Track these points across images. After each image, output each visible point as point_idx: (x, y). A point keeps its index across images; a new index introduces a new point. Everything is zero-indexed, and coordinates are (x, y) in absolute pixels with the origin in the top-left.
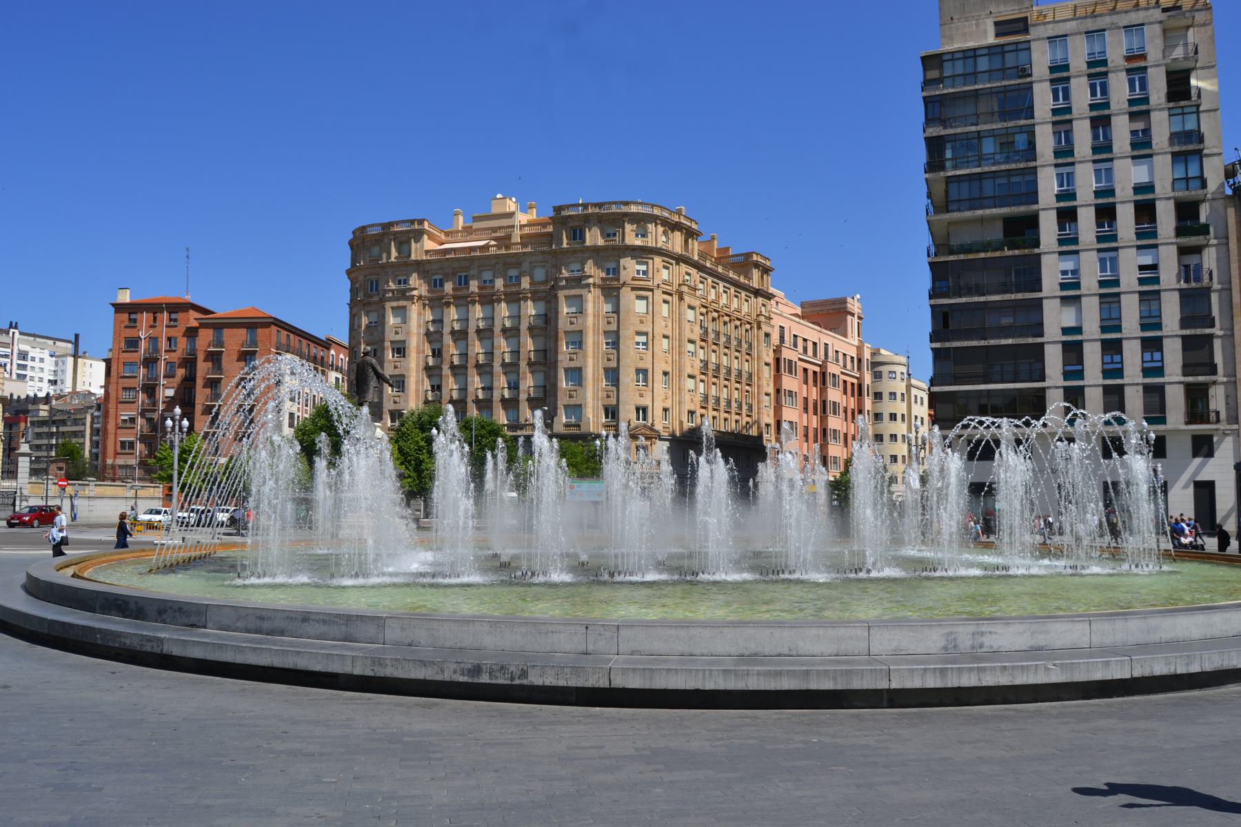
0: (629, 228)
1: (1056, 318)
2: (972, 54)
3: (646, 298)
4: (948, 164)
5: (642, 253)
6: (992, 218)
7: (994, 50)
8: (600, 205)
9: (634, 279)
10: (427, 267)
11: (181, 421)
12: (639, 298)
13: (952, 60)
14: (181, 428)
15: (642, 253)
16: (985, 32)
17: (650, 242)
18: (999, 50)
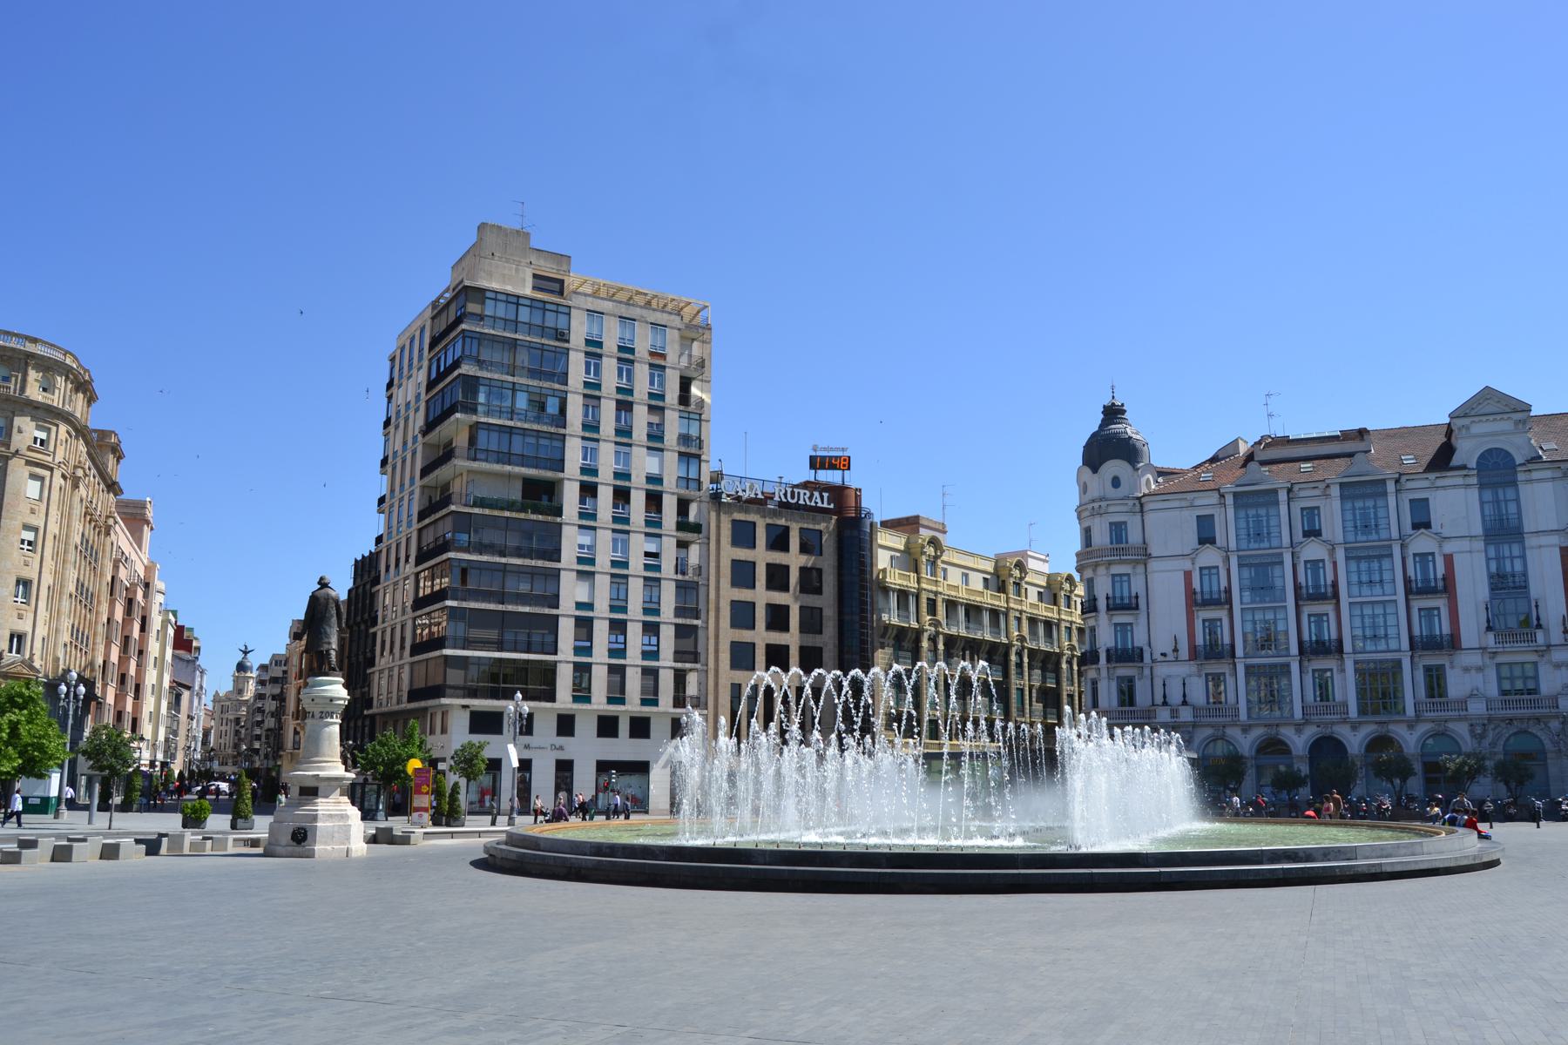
0: (33, 375)
1: (572, 591)
3: (42, 479)
5: (46, 414)
12: (33, 476)
15: (46, 414)
17: (55, 400)
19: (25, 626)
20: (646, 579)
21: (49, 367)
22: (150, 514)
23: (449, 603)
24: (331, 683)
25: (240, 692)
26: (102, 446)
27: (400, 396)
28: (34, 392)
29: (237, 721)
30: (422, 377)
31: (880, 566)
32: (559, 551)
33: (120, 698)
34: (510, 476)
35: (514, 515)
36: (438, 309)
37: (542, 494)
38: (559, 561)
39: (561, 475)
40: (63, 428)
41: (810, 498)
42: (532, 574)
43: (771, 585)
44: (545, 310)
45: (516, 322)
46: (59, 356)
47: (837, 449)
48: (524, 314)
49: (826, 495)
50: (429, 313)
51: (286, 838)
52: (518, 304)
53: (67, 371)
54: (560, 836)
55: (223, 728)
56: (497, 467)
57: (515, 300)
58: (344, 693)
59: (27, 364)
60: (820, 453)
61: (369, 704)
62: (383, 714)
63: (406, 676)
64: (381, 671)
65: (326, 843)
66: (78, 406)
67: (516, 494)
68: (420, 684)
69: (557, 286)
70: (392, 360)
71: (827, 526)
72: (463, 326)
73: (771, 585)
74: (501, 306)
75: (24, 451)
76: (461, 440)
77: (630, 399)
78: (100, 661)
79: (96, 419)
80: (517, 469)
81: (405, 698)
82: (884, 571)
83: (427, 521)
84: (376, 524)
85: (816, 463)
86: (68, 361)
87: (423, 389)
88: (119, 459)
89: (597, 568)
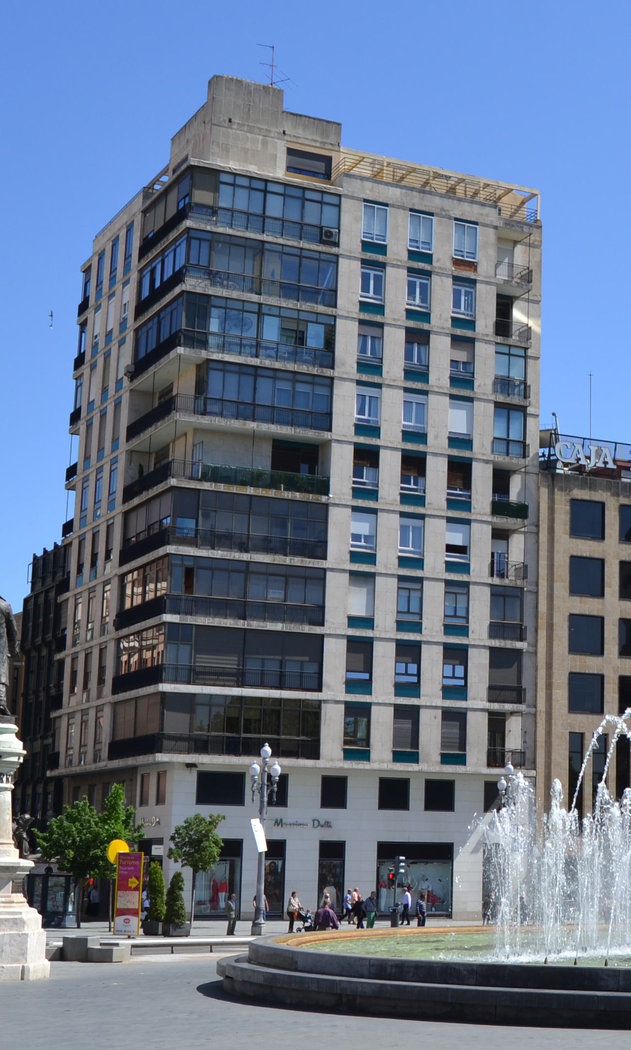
1: (343, 601)
2: (261, 186)
16: (274, 157)
18: (298, 193)
27: (98, 323)
30: (128, 295)
32: (324, 543)
35: (260, 492)
36: (153, 200)
37: (300, 462)
39: (327, 435)
52: (265, 192)
57: (262, 186)
61: (54, 761)
62: (74, 777)
63: (106, 722)
64: (71, 715)
67: (263, 462)
68: (126, 733)
69: (322, 166)
70: (87, 271)
72: (188, 223)
74: (242, 194)
76: (185, 386)
80: (264, 427)
81: (105, 753)
83: (136, 501)
87: (130, 313)
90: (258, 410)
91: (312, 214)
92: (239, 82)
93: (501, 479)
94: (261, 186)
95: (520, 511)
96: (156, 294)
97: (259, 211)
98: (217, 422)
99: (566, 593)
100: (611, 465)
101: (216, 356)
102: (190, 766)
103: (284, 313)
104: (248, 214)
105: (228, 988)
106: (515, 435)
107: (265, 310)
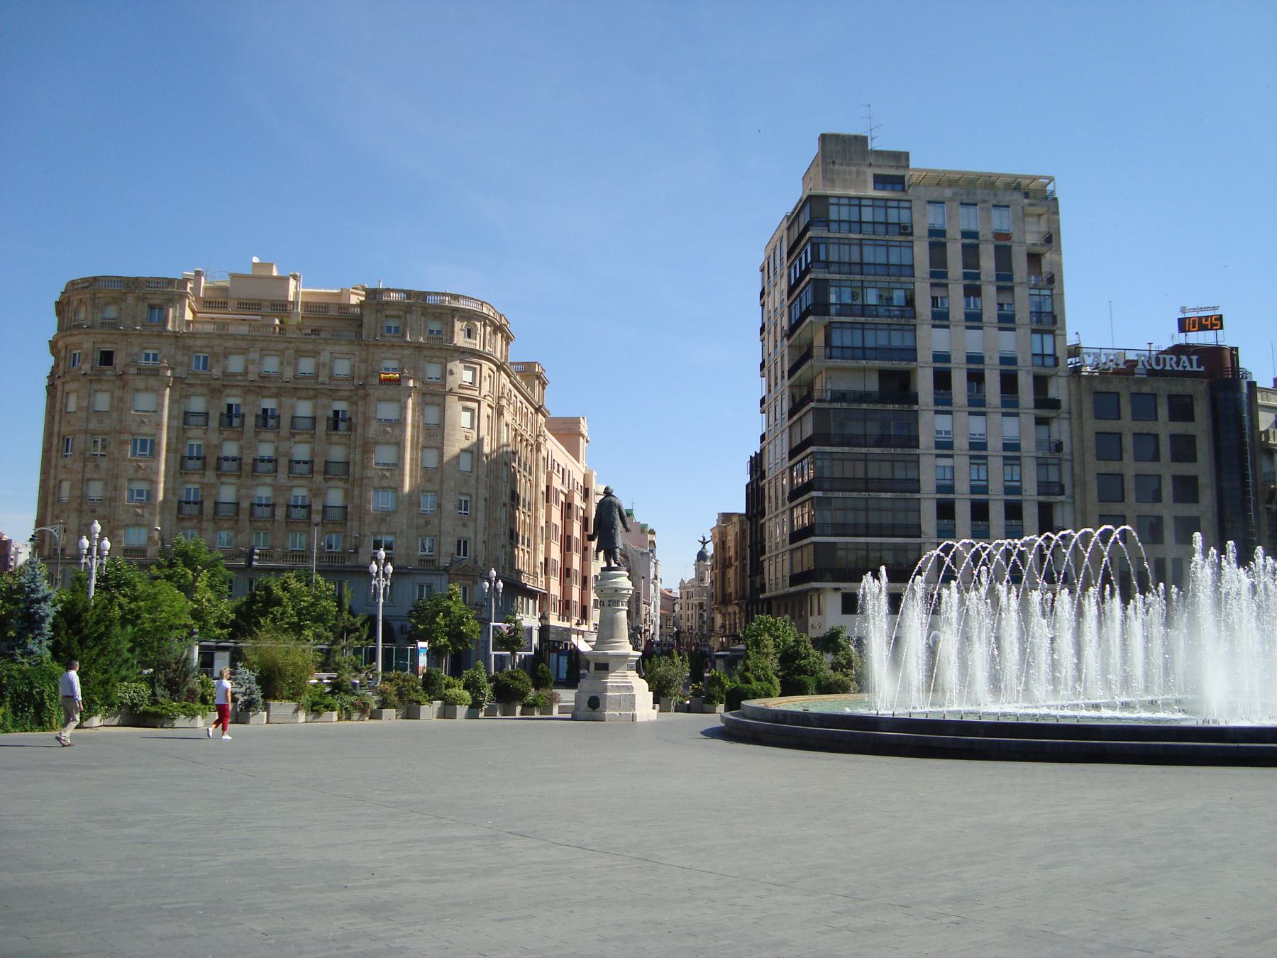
0: (459, 325)
1: (929, 476)
2: (856, 202)
3: (472, 410)
4: (833, 310)
5: (469, 356)
6: (872, 369)
7: (877, 203)
8: (456, 297)
9: (461, 387)
10: (189, 342)
11: (101, 539)
12: (465, 409)
13: (838, 204)
14: (99, 552)
15: (469, 356)
16: (865, 181)
17: (476, 344)
18: (882, 203)
19: (468, 533)
20: (1005, 458)
21: (469, 316)
22: (584, 428)
23: (814, 494)
24: (616, 576)
25: (702, 580)
26: (530, 374)
27: (769, 301)
28: (460, 340)
29: (701, 605)
30: (784, 286)
31: (1262, 428)
32: (917, 438)
33: (566, 590)
34: (864, 369)
35: (872, 406)
36: (793, 219)
37: (898, 386)
38: (917, 447)
39: (914, 364)
40: (486, 365)
41: (1178, 364)
42: (893, 462)
43: (1177, 457)
44: (887, 207)
45: (860, 222)
46: (476, 307)
47: (1207, 309)
48: (867, 215)
49: (1194, 358)
50: (785, 225)
51: (584, 705)
52: (860, 206)
53: (484, 318)
54: (848, 711)
55: (690, 612)
56: (851, 363)
57: (858, 202)
58: (628, 584)
59: (453, 317)
60: (1188, 315)
61: (763, 589)
62: (776, 598)
63: (787, 563)
64: (770, 559)
65: (615, 710)
66: (497, 347)
67: (873, 385)
68: (797, 570)
69: (897, 182)
70: (762, 270)
71: (1199, 391)
72: (809, 234)
73: (1177, 457)
74: (844, 210)
75: (456, 389)
76: (819, 340)
77: (977, 283)
78: (541, 558)
79: (518, 353)
80: (871, 363)
81: (787, 583)
82: (1267, 432)
83: (795, 418)
84: (758, 424)
85: (1183, 325)
86: (485, 311)
87: (785, 296)
88: (544, 384)
89: (989, 452)
90: (868, 353)
91: (893, 216)
92: (52, 377)
93: (1040, 383)
94: (856, 202)
95: (1055, 404)
96: (798, 281)
97: (856, 219)
98: (839, 363)
99: (1132, 459)
100: (1122, 366)
101: (837, 319)
102: (836, 589)
103: (879, 285)
104: (849, 222)
105: (712, 733)
106: (1049, 350)
107: (866, 284)
